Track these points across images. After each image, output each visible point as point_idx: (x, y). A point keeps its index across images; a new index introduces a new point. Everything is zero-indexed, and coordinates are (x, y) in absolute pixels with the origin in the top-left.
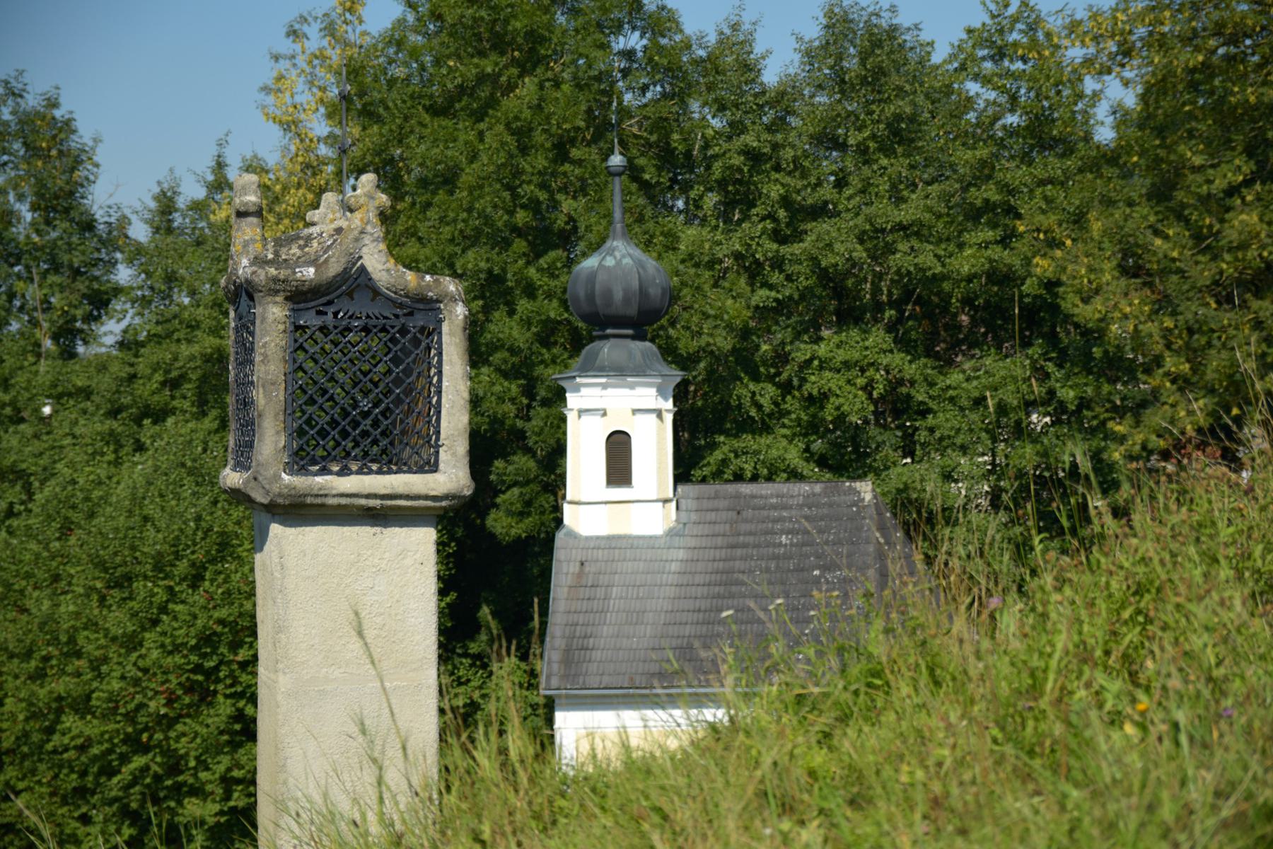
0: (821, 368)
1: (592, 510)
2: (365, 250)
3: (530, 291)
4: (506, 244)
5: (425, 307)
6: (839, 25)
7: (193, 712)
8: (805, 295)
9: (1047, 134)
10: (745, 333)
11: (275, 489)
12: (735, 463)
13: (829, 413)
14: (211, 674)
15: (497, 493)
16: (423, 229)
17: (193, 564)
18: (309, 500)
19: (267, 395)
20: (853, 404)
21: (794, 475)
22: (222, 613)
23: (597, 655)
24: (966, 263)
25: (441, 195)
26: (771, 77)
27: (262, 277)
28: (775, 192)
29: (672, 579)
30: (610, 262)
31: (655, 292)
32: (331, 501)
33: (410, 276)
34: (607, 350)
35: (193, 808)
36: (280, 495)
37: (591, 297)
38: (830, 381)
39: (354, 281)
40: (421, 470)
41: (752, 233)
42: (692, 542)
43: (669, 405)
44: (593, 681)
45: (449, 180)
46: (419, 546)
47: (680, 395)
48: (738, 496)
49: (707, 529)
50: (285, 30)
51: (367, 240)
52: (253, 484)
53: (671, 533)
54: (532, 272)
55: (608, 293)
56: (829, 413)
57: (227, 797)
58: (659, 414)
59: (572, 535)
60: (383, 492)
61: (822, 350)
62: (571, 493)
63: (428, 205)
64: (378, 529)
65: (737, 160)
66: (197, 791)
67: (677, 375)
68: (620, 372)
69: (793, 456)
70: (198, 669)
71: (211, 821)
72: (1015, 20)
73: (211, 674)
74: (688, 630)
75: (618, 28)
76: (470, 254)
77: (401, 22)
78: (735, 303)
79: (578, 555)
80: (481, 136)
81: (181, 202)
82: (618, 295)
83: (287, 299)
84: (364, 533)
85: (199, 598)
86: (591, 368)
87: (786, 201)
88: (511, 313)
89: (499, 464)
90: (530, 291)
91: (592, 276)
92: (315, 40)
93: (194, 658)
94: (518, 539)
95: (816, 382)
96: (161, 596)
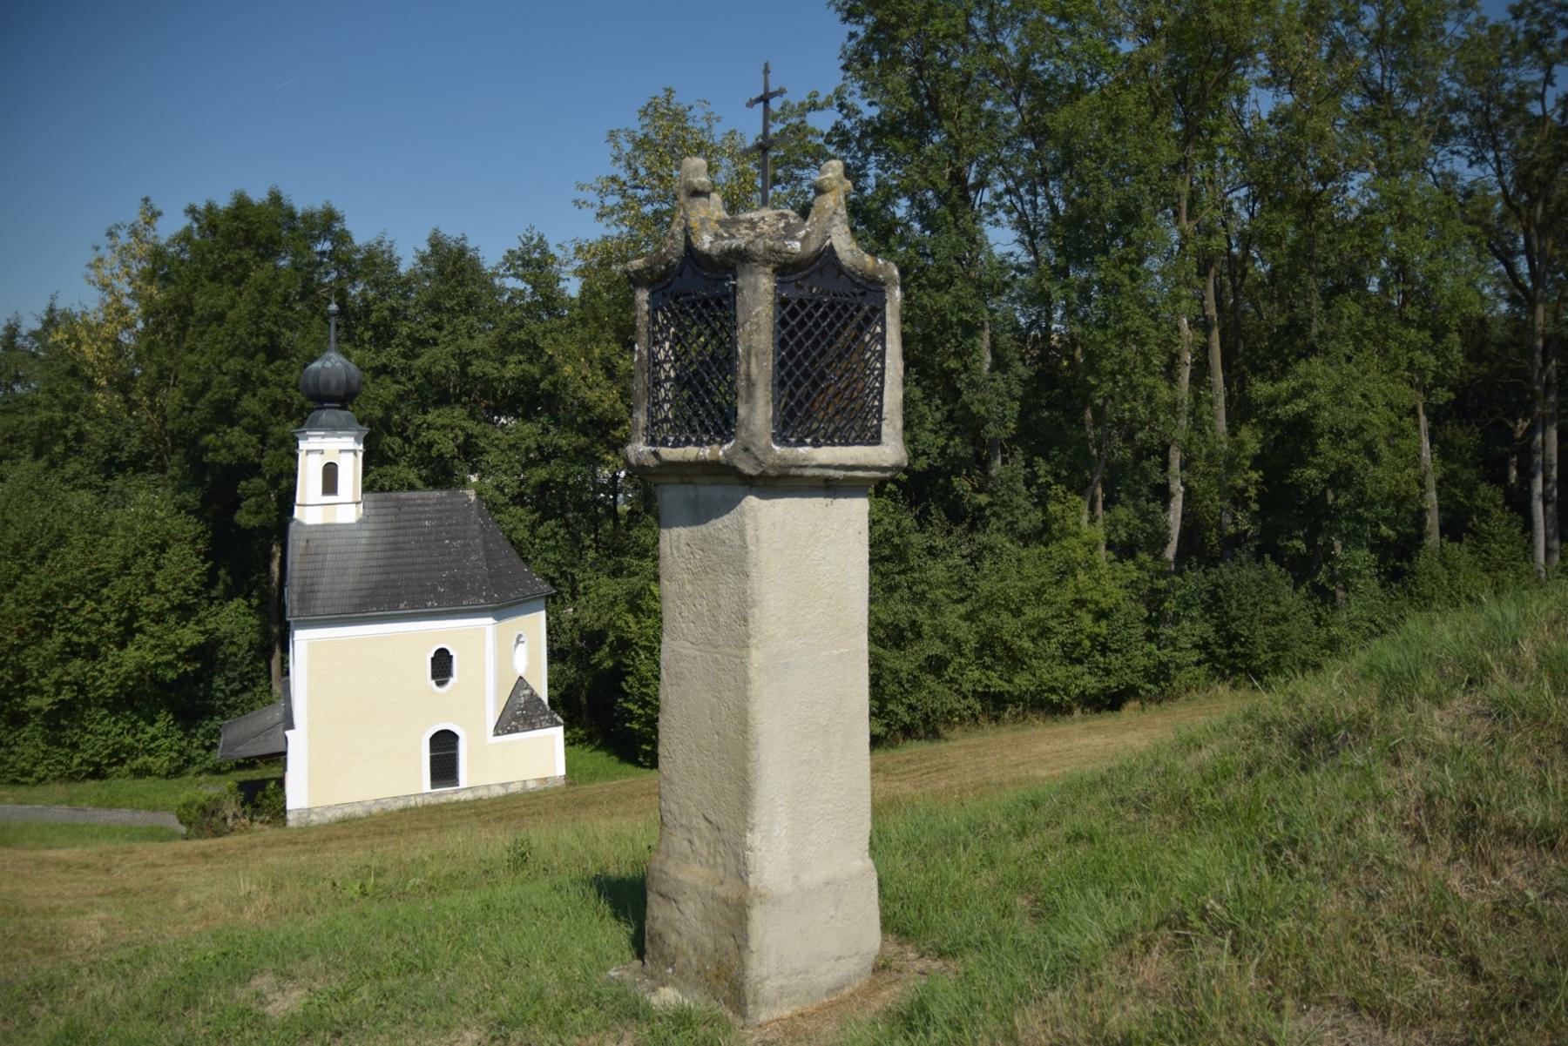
0: (428, 428)
1: (314, 508)
2: (834, 230)
3: (264, 382)
4: (251, 357)
5: (873, 287)
6: (436, 243)
7: (38, 641)
8: (419, 389)
9: (549, 302)
10: (387, 408)
11: (770, 460)
12: (380, 481)
13: (434, 453)
14: (50, 618)
15: (242, 500)
16: (200, 346)
17: (40, 549)
18: (793, 471)
19: (759, 364)
20: (447, 446)
21: (412, 487)
22: (61, 579)
23: (320, 595)
24: (510, 372)
25: (214, 326)
26: (404, 268)
27: (761, 246)
28: (405, 331)
29: (362, 548)
30: (328, 365)
31: (354, 382)
32: (809, 472)
33: (868, 258)
34: (325, 416)
35: (34, 701)
36: (772, 466)
37: (316, 385)
38: (434, 435)
39: (826, 258)
40: (869, 444)
41: (391, 355)
42: (374, 527)
43: (361, 447)
44: (320, 611)
45: (220, 318)
46: (851, 518)
47: (367, 441)
48: (398, 499)
49: (381, 519)
50: (186, 206)
51: (837, 220)
52: (742, 455)
53: (360, 522)
54: (266, 373)
55: (327, 383)
56: (434, 453)
57: (58, 693)
58: (355, 452)
59: (300, 524)
60: (850, 463)
61: (429, 418)
62: (298, 500)
63: (204, 332)
64: (829, 500)
65: (386, 313)
66: (39, 691)
67: (366, 430)
68: (333, 429)
69: (412, 476)
70: (41, 614)
71: (47, 709)
72: (536, 247)
73: (50, 618)
74: (374, 578)
75: (317, 239)
76: (231, 361)
77: (189, 229)
78: (388, 390)
79: (305, 536)
80: (240, 294)
81: (24, 331)
82: (333, 383)
83: (775, 271)
84: (816, 504)
85: (43, 570)
86: (317, 426)
87: (409, 336)
88: (254, 395)
89: (243, 483)
90: (264, 382)
91: (318, 373)
92: (124, 238)
93: (39, 608)
94: (254, 528)
95: (425, 436)
96: (17, 570)
